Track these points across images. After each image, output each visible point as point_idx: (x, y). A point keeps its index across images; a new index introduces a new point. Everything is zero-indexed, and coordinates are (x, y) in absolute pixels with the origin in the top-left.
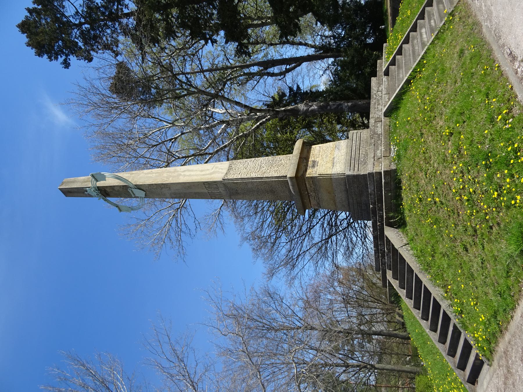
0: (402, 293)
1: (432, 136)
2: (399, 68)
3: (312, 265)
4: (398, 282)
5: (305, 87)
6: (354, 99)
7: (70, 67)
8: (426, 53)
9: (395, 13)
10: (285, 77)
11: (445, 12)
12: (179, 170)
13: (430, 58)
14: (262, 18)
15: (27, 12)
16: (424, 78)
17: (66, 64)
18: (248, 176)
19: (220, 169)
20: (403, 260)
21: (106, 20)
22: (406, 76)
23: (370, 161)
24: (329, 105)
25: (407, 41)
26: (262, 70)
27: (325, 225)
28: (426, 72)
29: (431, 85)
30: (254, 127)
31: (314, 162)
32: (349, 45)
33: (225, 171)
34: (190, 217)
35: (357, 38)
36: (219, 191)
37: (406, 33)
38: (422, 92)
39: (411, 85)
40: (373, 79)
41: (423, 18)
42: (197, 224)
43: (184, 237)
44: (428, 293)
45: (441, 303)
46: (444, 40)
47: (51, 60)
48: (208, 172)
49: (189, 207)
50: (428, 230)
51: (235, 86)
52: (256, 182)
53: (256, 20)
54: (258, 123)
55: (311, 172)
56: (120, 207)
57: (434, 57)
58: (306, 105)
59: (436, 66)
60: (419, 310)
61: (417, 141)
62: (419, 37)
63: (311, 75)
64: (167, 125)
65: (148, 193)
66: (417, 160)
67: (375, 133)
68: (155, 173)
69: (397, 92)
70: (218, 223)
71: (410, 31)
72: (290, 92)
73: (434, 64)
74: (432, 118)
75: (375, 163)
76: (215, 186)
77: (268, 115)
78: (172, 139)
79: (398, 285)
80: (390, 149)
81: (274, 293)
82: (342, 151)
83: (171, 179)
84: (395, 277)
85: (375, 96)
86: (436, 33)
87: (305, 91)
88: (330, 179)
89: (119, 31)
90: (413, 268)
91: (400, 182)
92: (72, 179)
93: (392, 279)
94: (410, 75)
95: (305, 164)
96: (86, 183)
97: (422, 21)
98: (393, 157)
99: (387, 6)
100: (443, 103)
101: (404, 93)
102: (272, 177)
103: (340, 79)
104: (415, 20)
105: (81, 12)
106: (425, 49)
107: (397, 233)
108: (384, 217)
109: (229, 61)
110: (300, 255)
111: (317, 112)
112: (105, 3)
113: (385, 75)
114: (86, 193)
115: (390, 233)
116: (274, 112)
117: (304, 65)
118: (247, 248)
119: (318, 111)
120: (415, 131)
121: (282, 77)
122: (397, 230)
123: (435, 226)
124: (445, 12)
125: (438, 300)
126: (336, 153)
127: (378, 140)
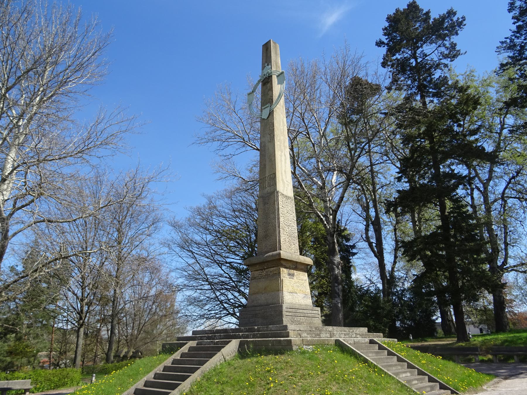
0: (177, 355)
1: (323, 381)
2: (377, 353)
3: (182, 266)
4: (187, 351)
5: (355, 261)
6: (344, 310)
7: (377, 46)
8: (390, 376)
9: (424, 349)
10: (365, 241)
11: (424, 392)
12: (286, 150)
13: (386, 379)
14: (420, 222)
15: (427, 11)
16: (370, 374)
17: (379, 44)
18: (281, 215)
19: (287, 188)
20: (211, 357)
21: (419, 82)
22: (371, 359)
24: (339, 285)
25: (400, 360)
26: (371, 219)
27: (221, 279)
28: (374, 376)
29: (364, 380)
30: (319, 213)
31: (293, 275)
32: (394, 305)
33: (285, 193)
34: (235, 150)
35: (401, 312)
36: (266, 186)
37: (406, 360)
38: (358, 373)
39: (364, 363)
40: (366, 329)
41: (419, 374)
42: (227, 158)
43: (216, 144)
44: (184, 378)
45: (177, 390)
46: (401, 391)
47: (383, 30)
48: (284, 177)
49: (244, 149)
50: (242, 378)
51: (357, 193)
52: (276, 222)
53: (418, 215)
54: (322, 217)
55: (284, 272)
56: (252, 94)
57: (387, 383)
58: (339, 263)
59: (380, 384)
60: (163, 371)
61: (318, 368)
62: (403, 370)
63: (365, 266)
64: (321, 130)
65: (266, 121)
66: (303, 368)
69: (357, 351)
70: (227, 175)
71: (408, 363)
72: (350, 246)
73: (382, 383)
74: (337, 381)
75: (296, 332)
76: (272, 184)
77: (330, 226)
78: (309, 135)
79: (184, 352)
80: (309, 345)
81: (156, 227)
83: (279, 143)
84: (191, 349)
85: (351, 331)
86: (407, 385)
87: (351, 261)
88: (278, 289)
89: (409, 92)
90: (205, 365)
91: (282, 353)
92: (279, 52)
93: (189, 346)
94: (372, 363)
95: (291, 267)
96: (275, 65)
97: (416, 373)
98: (303, 348)
99: (430, 341)
100: (351, 390)
101: (356, 357)
102: (280, 237)
103: (363, 295)
104: (417, 367)
105: (426, 58)
106: (393, 375)
107: (234, 351)
108: (249, 340)
109: (380, 188)
110: (192, 253)
111: (332, 273)
112: (434, 82)
113: (370, 340)
114: (266, 64)
115: (233, 345)
116: (333, 233)
117: (376, 260)
118: (202, 202)
119: (333, 275)
120: (326, 367)
121: (365, 238)
122: (236, 351)
123: (247, 384)
124: (424, 392)
125: (179, 387)
126: (301, 295)
127: (315, 334)
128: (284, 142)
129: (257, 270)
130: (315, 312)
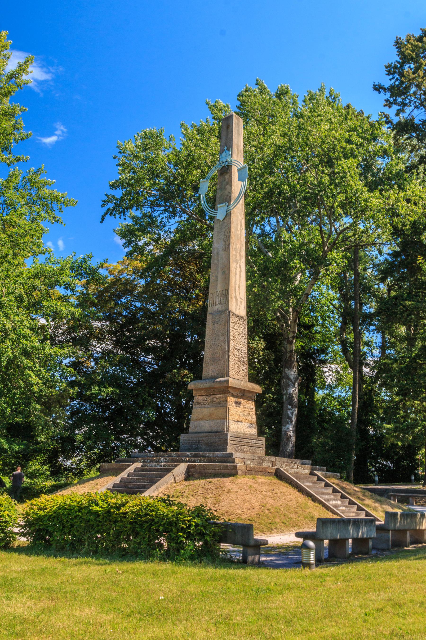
2: (314, 483)
18: (231, 338)
23: (242, 456)
31: (240, 403)
33: (237, 313)
36: (217, 303)
67: (263, 460)
68: (241, 234)
82: (247, 430)
88: (225, 417)
108: (197, 464)
114: (226, 148)
126: (247, 424)
128: (240, 251)
129: (202, 396)
130: (259, 442)
